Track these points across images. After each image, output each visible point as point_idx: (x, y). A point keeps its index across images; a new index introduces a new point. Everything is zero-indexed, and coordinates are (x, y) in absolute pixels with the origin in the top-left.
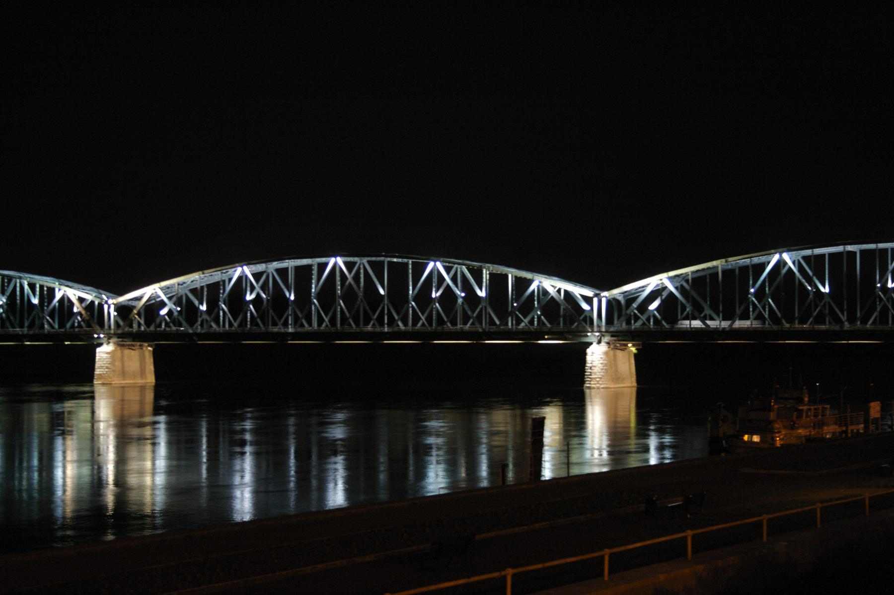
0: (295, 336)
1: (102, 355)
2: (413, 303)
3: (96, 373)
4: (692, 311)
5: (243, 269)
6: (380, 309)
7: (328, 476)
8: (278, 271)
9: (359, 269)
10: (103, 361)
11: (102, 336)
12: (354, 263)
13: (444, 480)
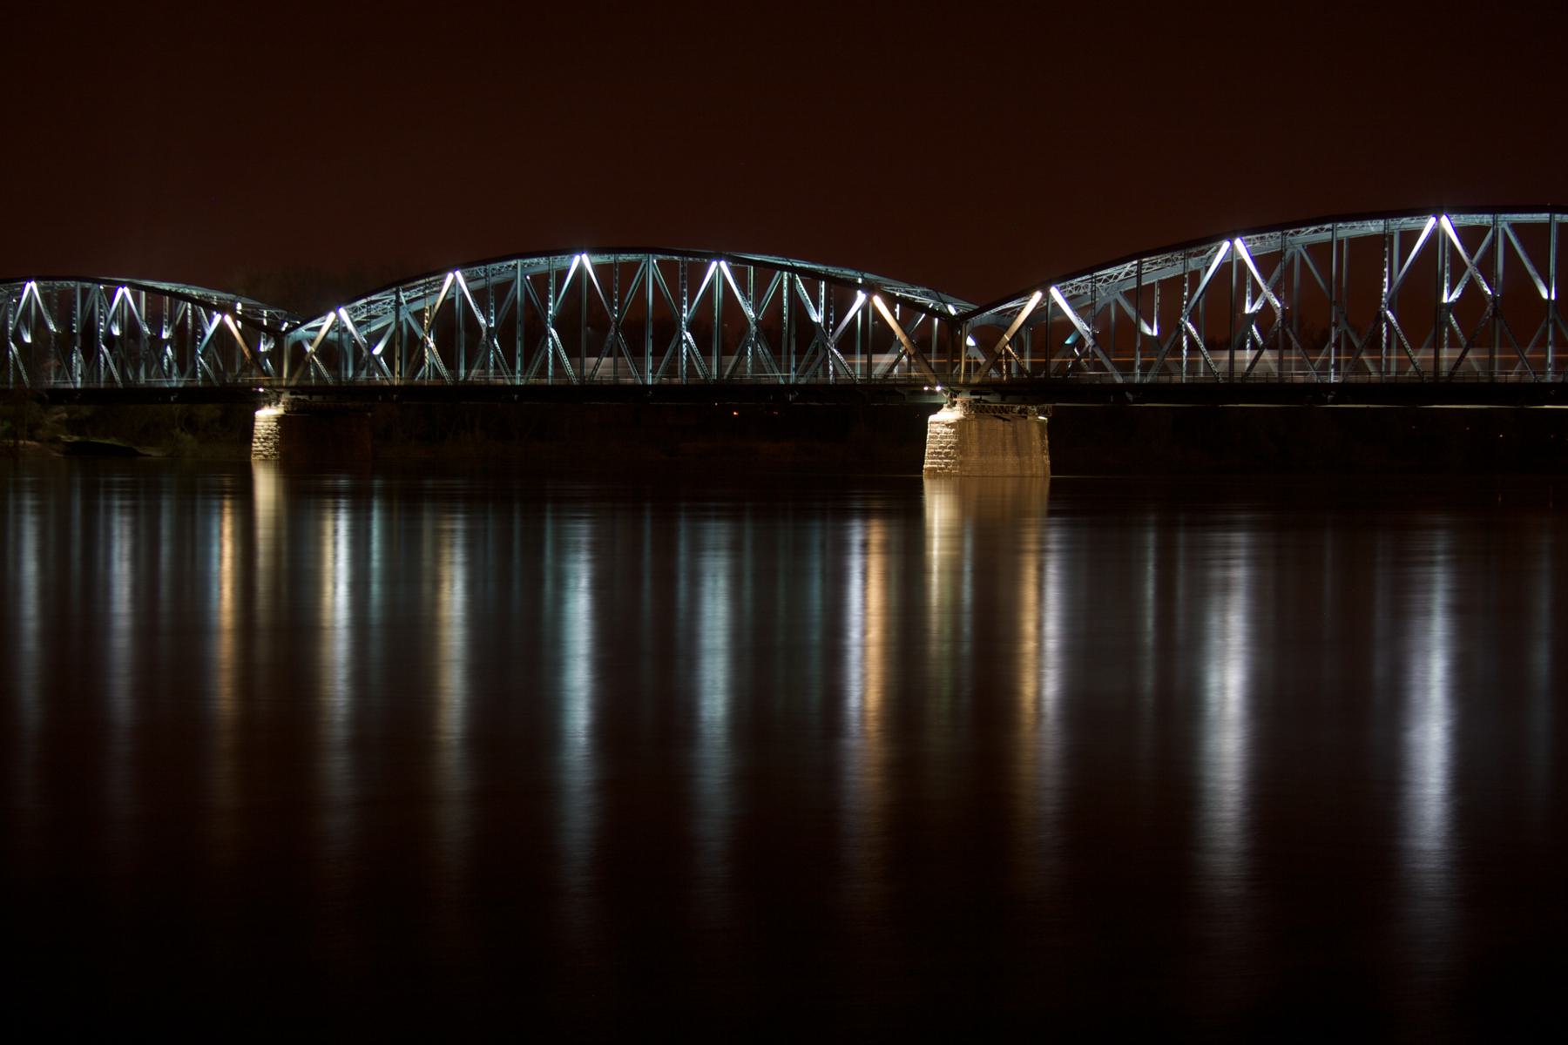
0: (1343, 391)
1: (938, 430)
2: (688, 334)
3: (925, 466)
4: (1094, 346)
5: (482, 278)
6: (1539, 332)
7: (1239, 739)
8: (1312, 248)
9: (1494, 240)
10: (941, 442)
11: (938, 389)
12: (1481, 231)
13: (1227, 740)
